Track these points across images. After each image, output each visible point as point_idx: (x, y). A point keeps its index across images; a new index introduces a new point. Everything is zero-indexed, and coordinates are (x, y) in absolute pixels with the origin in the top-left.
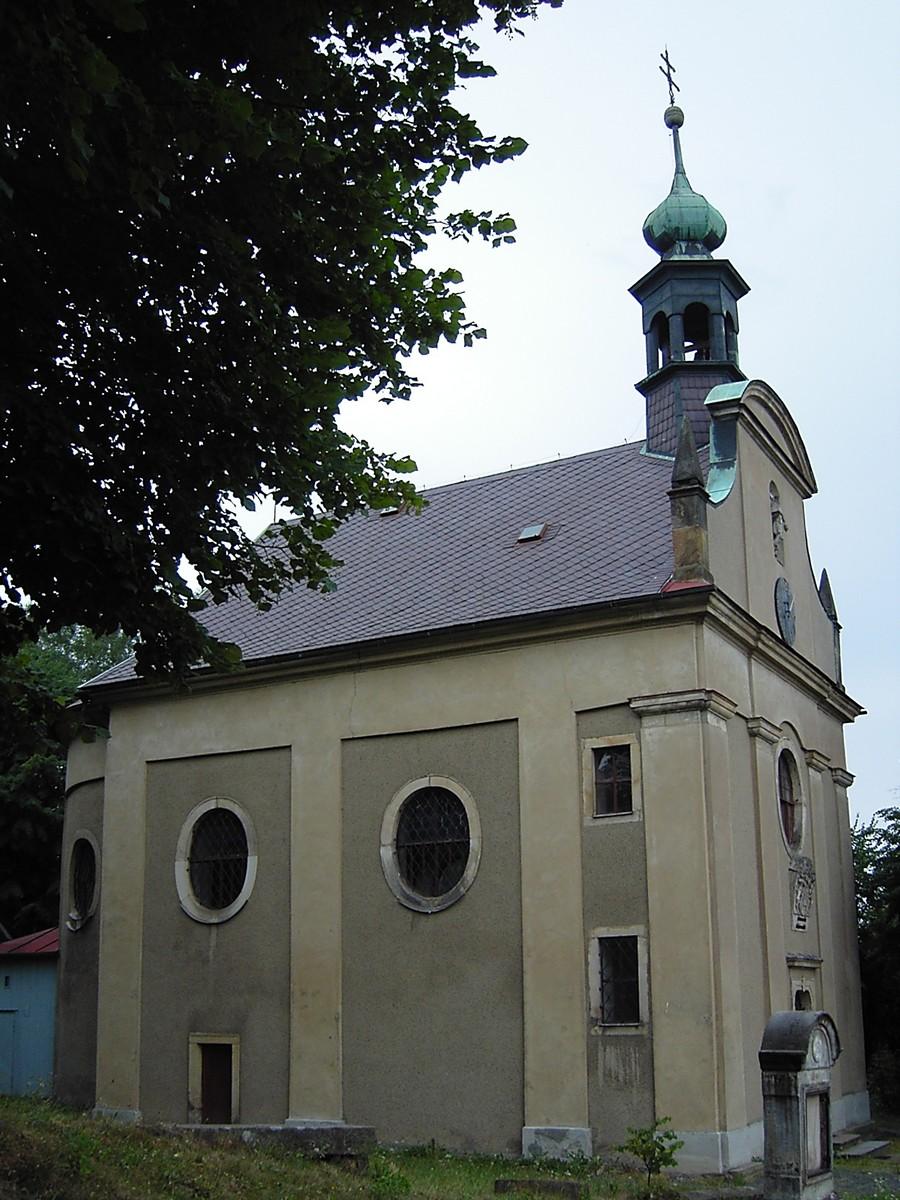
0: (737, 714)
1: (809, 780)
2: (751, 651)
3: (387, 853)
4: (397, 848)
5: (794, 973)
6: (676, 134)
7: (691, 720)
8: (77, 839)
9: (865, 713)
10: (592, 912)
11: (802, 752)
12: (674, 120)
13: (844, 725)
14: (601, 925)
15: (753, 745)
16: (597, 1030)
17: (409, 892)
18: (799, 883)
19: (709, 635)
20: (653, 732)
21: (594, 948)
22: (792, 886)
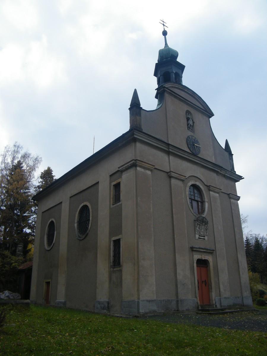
0: (222, 192)
1: (210, 195)
2: (168, 153)
3: (76, 225)
4: (79, 223)
5: (194, 253)
6: (165, 38)
7: (132, 172)
8: (196, 260)
9: (243, 178)
10: (111, 234)
11: (205, 187)
12: (165, 33)
13: (236, 183)
14: (114, 236)
15: (170, 180)
16: (112, 269)
17: (80, 235)
18: (198, 224)
19: (138, 145)
20: (125, 176)
21: (112, 242)
22: (195, 225)
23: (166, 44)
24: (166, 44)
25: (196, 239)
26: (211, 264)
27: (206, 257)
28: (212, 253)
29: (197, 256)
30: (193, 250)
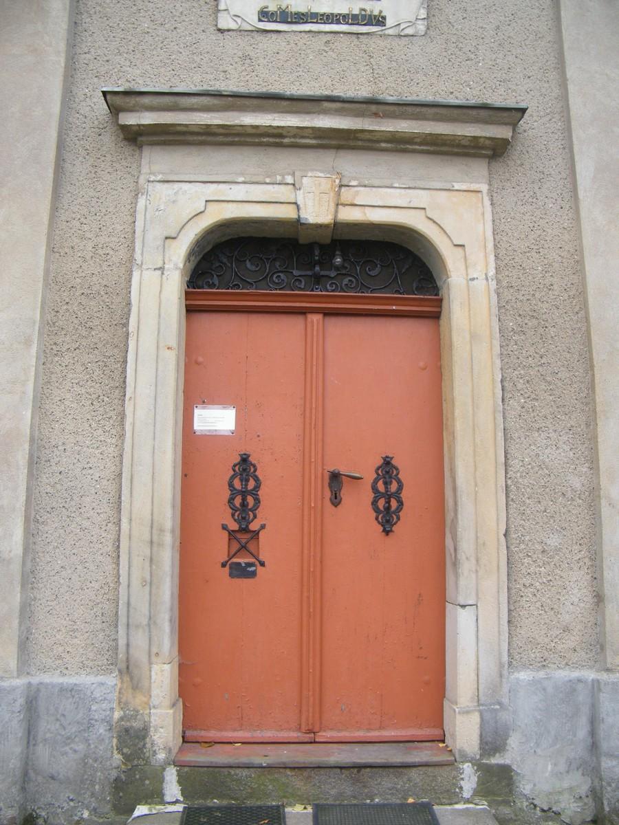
5: (157, 161)
23: (336, 216)
24: (336, 216)
25: (225, 22)
26: (469, 282)
27: (364, 196)
28: (495, 152)
29: (192, 199)
30: (135, 138)
